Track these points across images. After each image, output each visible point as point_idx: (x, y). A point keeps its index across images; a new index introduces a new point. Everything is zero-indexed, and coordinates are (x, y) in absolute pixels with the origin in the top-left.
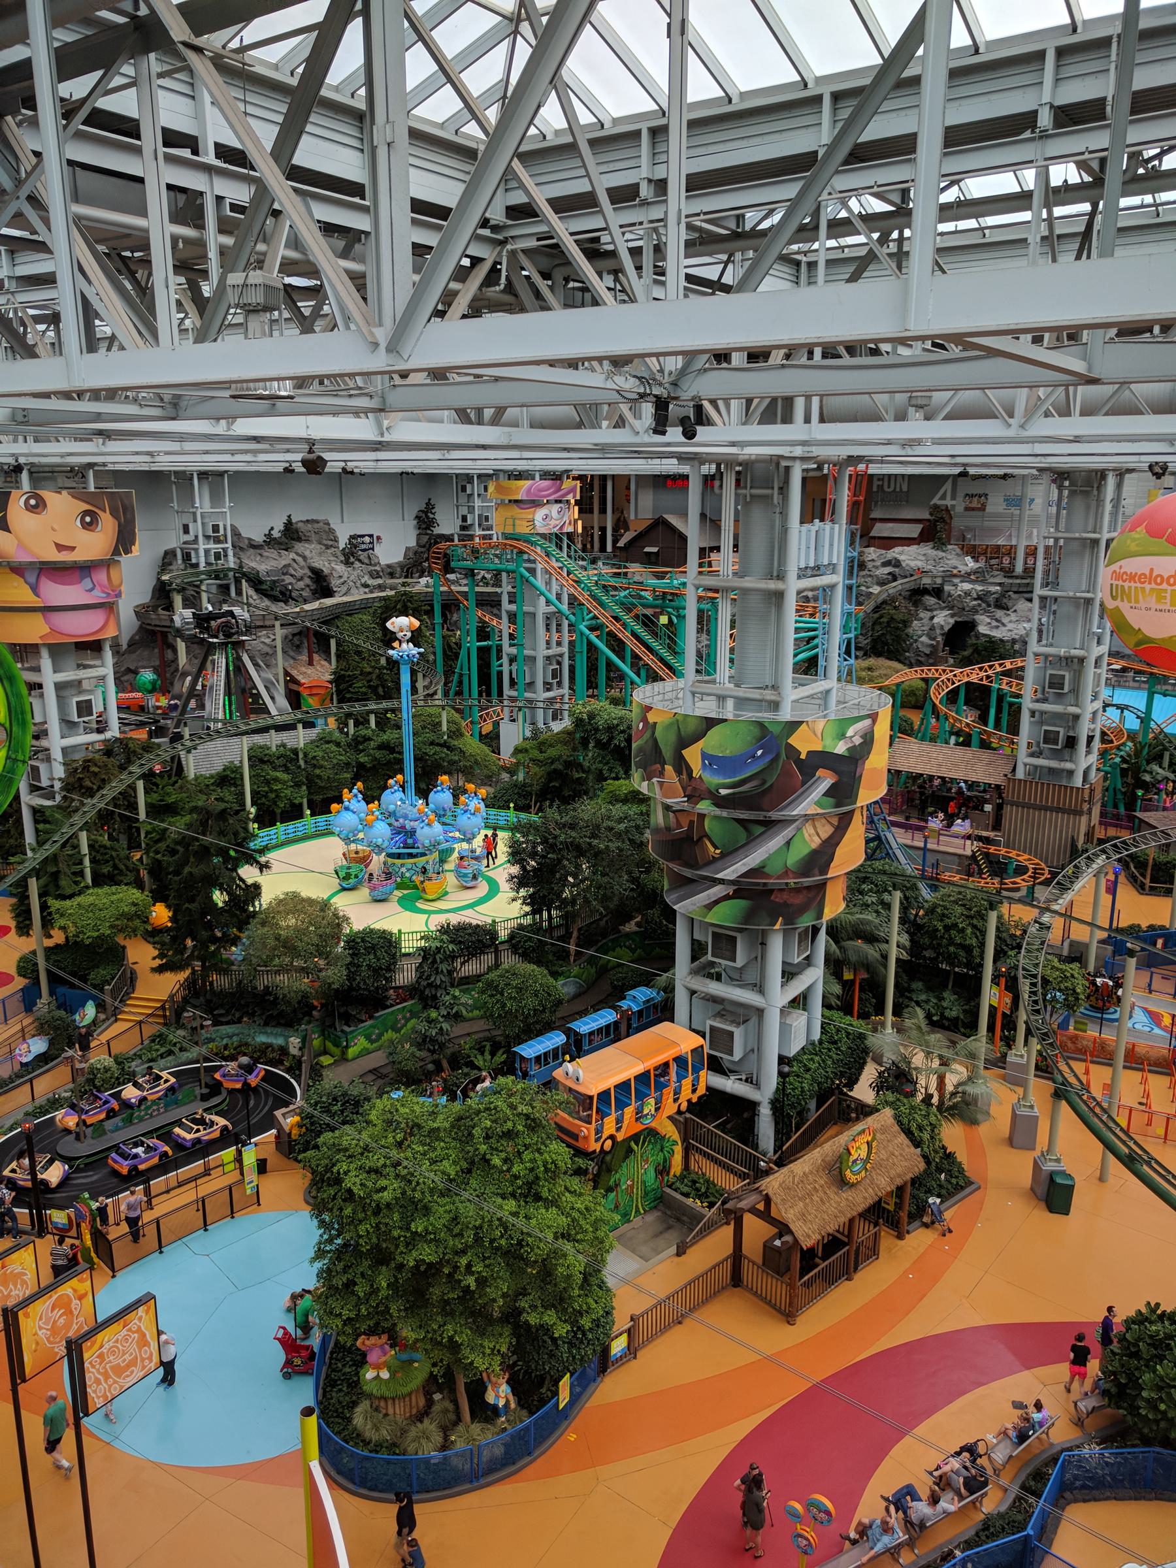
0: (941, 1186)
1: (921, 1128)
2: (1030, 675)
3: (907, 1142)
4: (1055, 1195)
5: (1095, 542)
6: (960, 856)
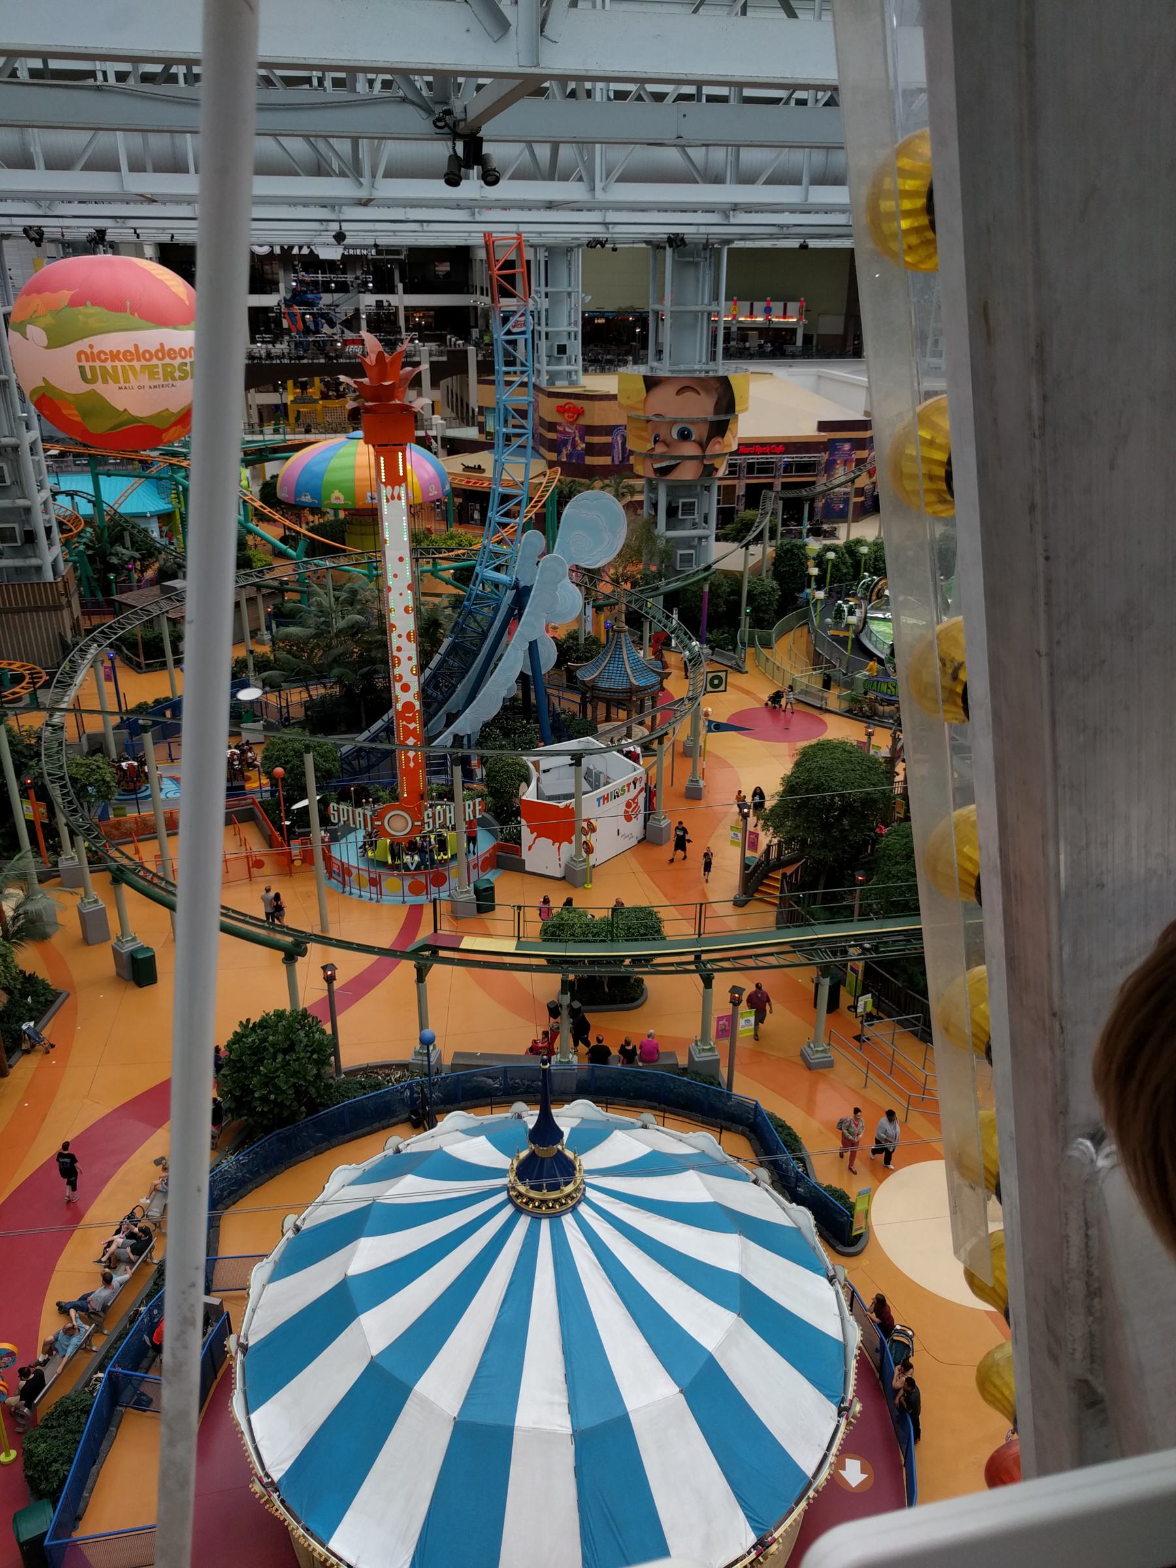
4: (140, 970)
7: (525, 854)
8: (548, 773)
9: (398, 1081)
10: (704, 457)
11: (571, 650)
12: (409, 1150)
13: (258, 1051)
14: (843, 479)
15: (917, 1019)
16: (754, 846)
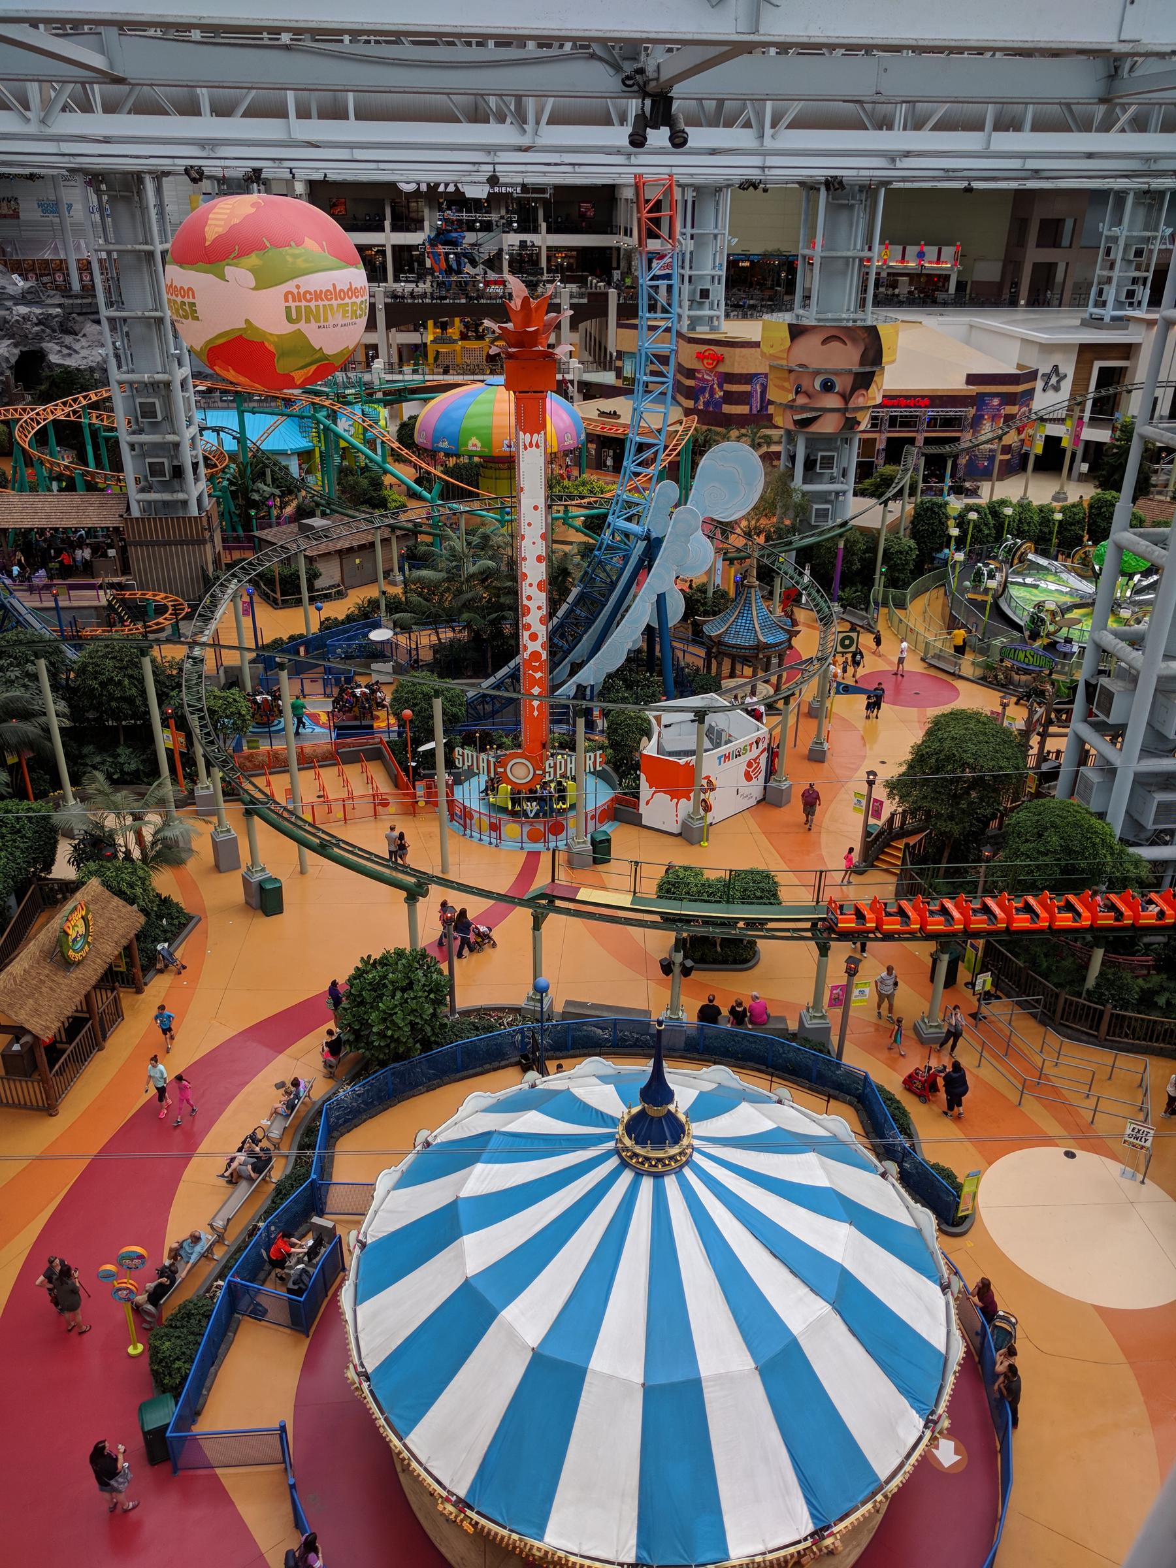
0: (165, 931)
1: (131, 886)
2: (119, 403)
3: (122, 902)
4: (266, 900)
6: (96, 608)
7: (643, 809)
9: (510, 1024)
10: (846, 410)
12: (439, 1140)
13: (377, 988)
14: (989, 436)
15: (1037, 1001)
16: (877, 814)
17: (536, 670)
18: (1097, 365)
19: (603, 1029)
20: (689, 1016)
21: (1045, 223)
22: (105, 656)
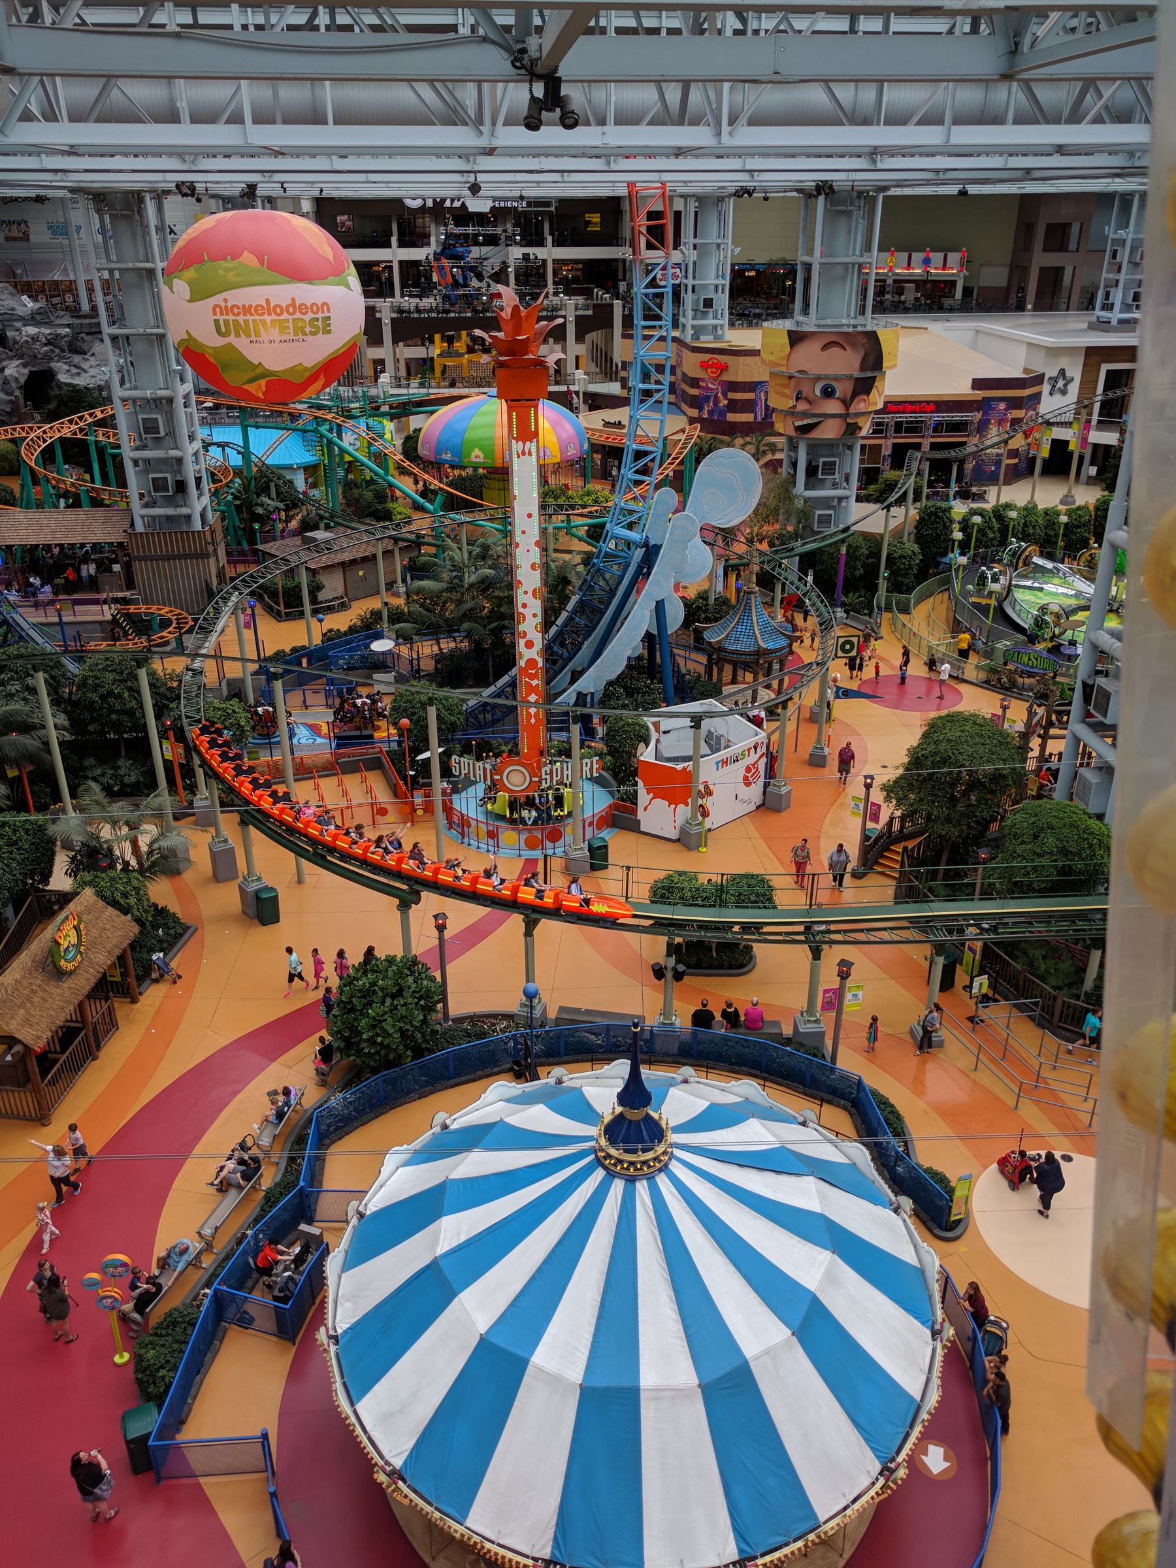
0: (161, 941)
1: (125, 895)
2: (122, 422)
3: (115, 912)
4: (263, 909)
5: (151, 272)
6: (100, 622)
7: (641, 815)
8: (668, 734)
9: (503, 1031)
11: (700, 611)
15: (1035, 1004)
17: (533, 677)
18: (1105, 368)
19: (597, 1035)
20: (682, 1021)
21: (1050, 227)
22: (105, 669)
